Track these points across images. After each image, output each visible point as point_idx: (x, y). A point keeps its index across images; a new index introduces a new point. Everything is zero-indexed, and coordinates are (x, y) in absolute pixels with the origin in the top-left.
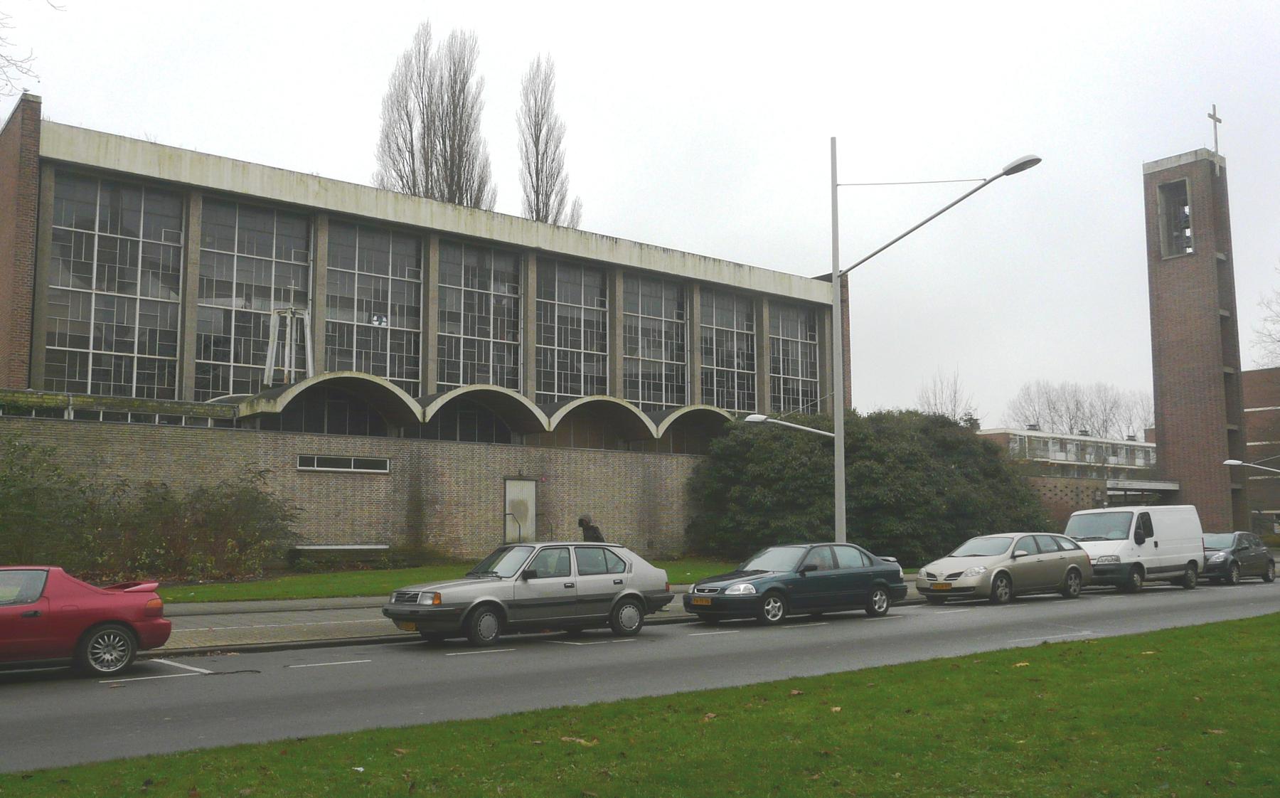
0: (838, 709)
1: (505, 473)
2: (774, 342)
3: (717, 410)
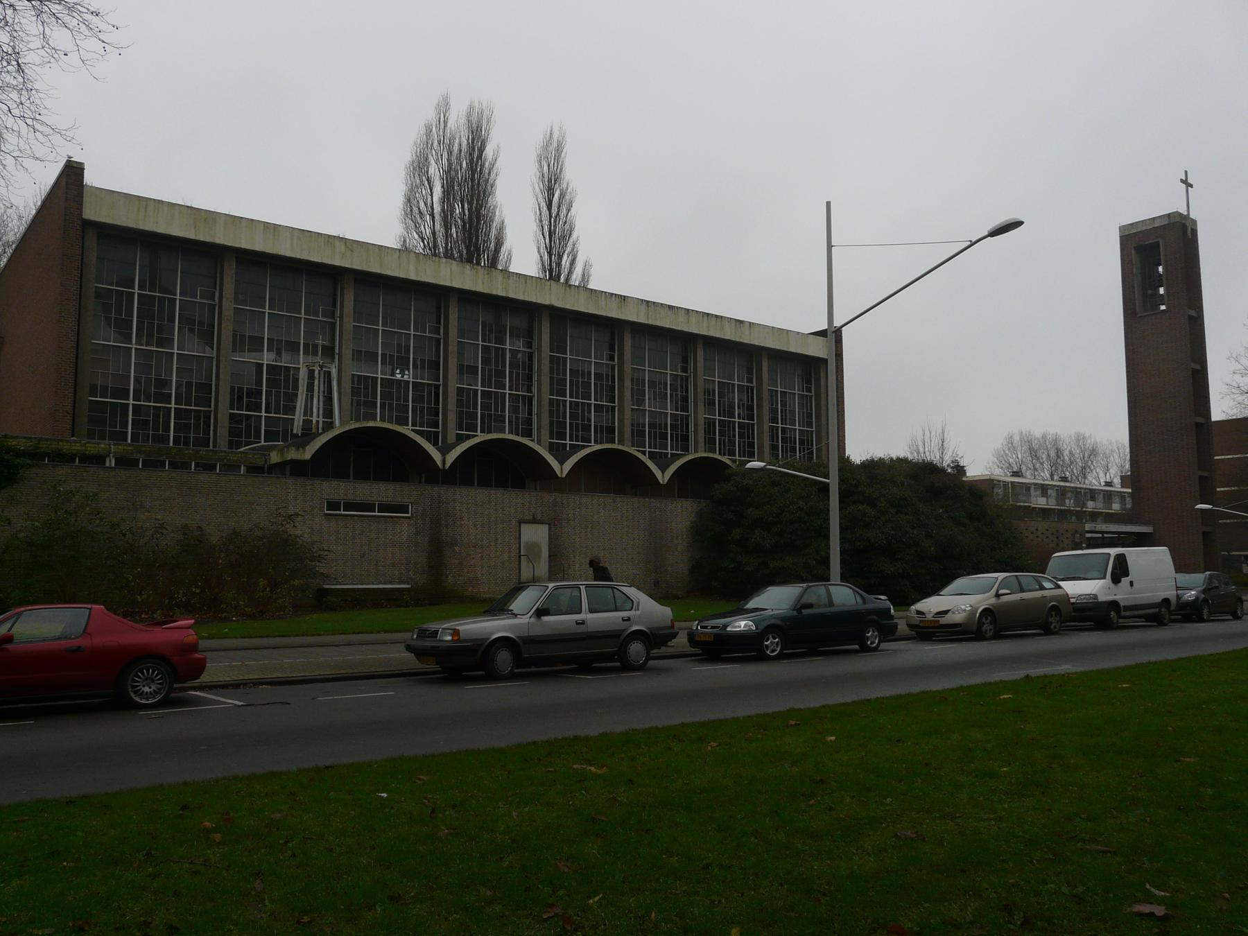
2: (773, 393)
3: (719, 457)
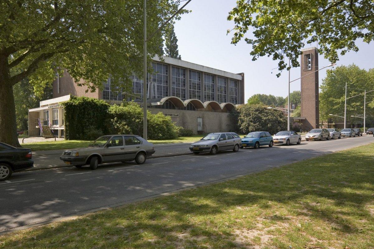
3: (232, 104)
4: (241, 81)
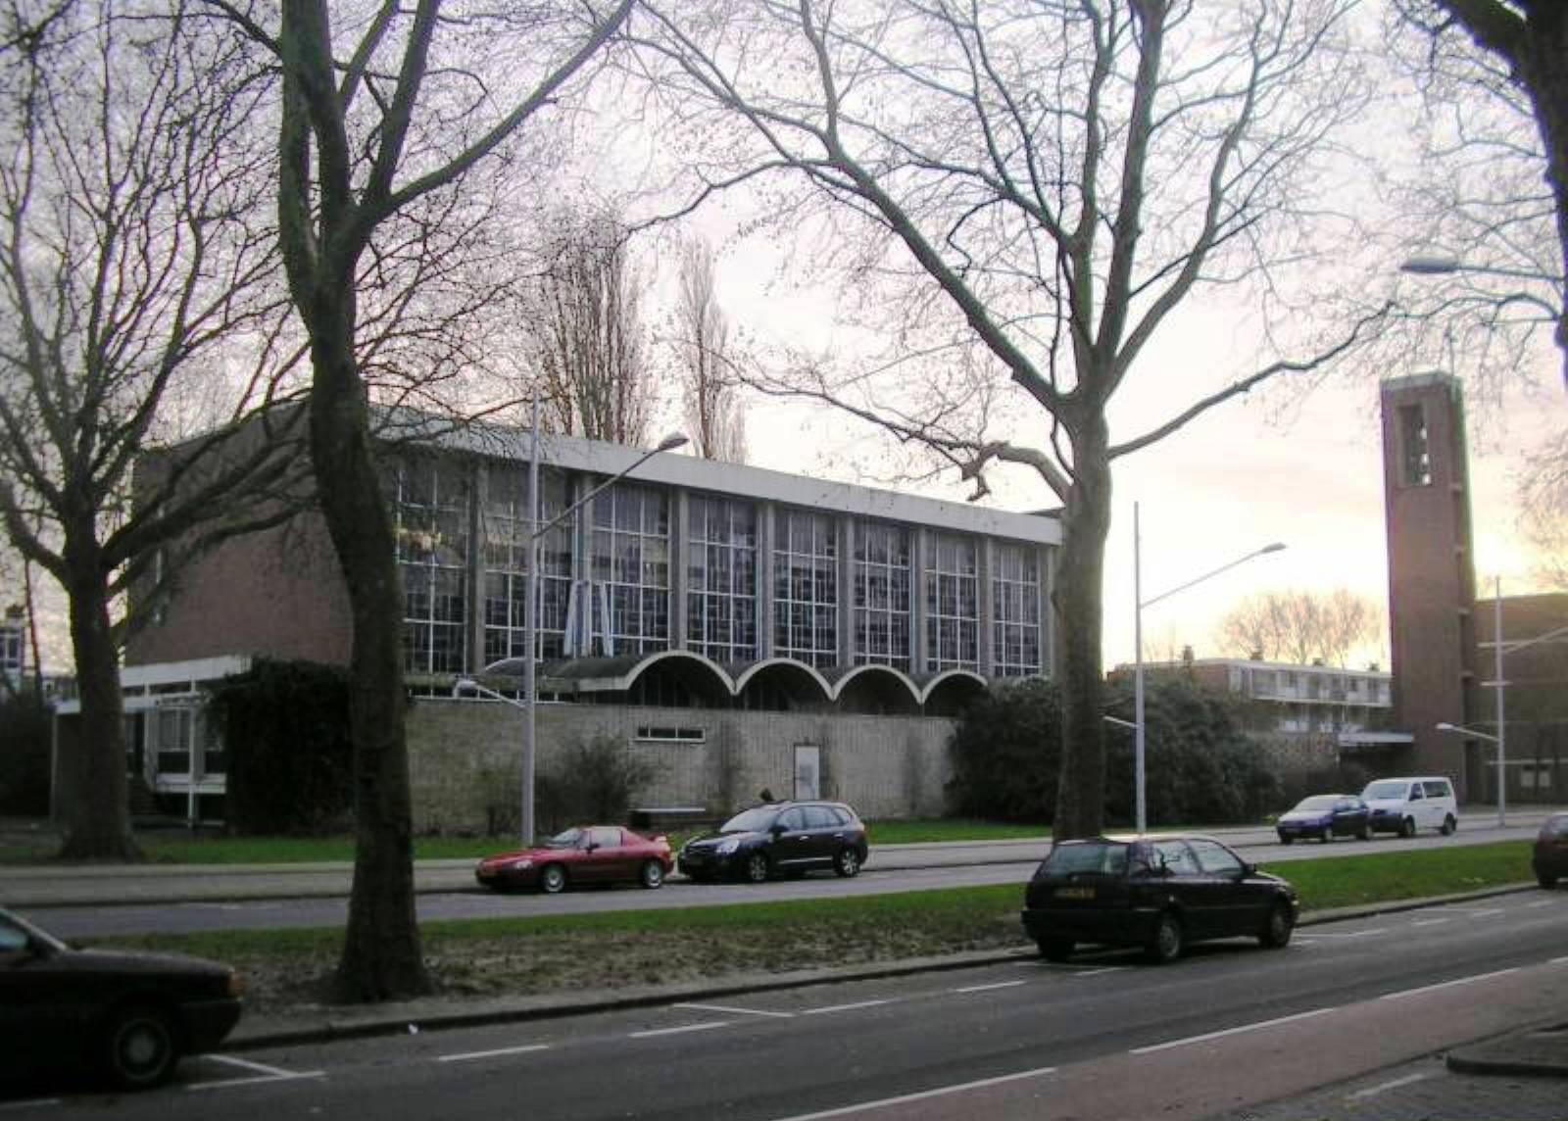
0: (1442, 726)
1: (796, 740)
2: (997, 585)
4: (1054, 547)
